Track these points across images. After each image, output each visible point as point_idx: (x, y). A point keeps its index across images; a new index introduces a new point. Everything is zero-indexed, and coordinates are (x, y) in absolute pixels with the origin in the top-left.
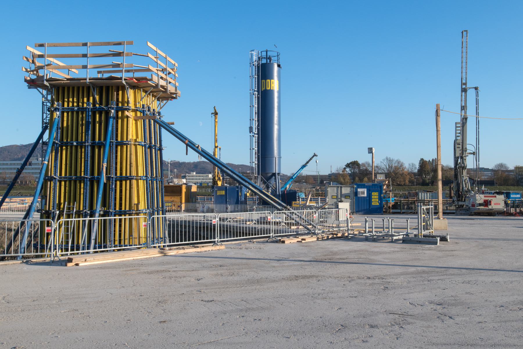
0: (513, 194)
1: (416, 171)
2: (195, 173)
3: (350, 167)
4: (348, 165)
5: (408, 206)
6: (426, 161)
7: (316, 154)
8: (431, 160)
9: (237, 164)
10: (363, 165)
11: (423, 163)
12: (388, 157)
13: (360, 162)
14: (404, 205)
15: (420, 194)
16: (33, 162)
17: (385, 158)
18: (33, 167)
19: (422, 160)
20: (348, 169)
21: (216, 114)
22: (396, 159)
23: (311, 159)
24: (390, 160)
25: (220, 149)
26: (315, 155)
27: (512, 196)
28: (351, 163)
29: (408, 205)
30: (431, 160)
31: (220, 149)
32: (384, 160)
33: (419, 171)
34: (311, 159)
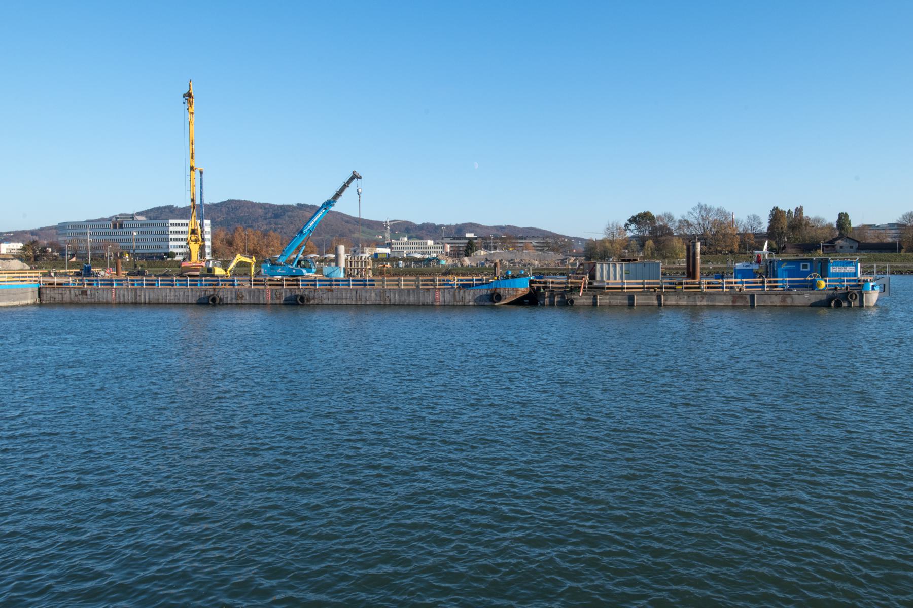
0: (835, 264)
1: (766, 230)
2: (406, 239)
3: (636, 222)
4: (633, 220)
5: (563, 297)
6: (782, 212)
7: (359, 172)
8: (793, 210)
9: (521, 226)
10: (660, 218)
11: (776, 215)
12: (703, 204)
13: (655, 213)
14: (552, 296)
15: (598, 266)
16: (125, 223)
17: (696, 205)
18: (125, 230)
19: (776, 209)
20: (632, 227)
21: (189, 95)
22: (716, 207)
23: (345, 186)
24: (704, 210)
25: (201, 173)
26: (355, 177)
27: (832, 269)
28: (639, 216)
29: (562, 295)
30: (793, 210)
31: (201, 173)
32: (693, 209)
33: (769, 229)
34: (345, 186)
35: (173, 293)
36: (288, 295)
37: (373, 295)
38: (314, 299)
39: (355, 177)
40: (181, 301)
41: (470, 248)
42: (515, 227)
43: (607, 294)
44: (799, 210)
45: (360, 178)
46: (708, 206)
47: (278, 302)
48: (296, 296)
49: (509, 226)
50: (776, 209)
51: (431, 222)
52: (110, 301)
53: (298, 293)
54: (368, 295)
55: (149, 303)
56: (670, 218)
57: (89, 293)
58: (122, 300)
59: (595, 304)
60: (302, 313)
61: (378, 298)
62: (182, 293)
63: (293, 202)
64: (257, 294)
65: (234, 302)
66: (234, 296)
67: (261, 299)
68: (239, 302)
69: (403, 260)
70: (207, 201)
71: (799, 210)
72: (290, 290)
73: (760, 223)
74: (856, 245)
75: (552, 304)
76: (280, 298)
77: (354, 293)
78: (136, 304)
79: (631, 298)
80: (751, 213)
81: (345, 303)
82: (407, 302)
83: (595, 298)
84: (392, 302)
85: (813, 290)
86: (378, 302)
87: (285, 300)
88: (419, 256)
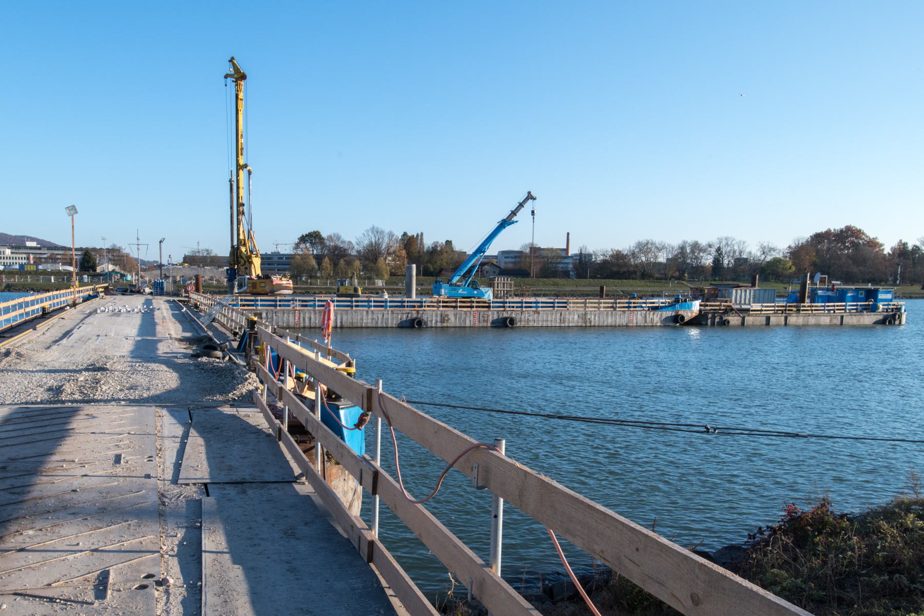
4: (303, 239)
14: (714, 318)
23: (521, 205)
26: (530, 197)
34: (521, 205)
35: (370, 316)
36: (496, 317)
37: (576, 317)
39: (530, 197)
40: (380, 325)
42: (6, 235)
43: (752, 315)
47: (485, 324)
48: (506, 318)
52: (292, 324)
53: (505, 315)
54: (571, 317)
55: (342, 327)
57: (264, 315)
58: (307, 324)
59: (743, 324)
60: (508, 335)
61: (580, 321)
62: (380, 316)
64: (463, 316)
65: (439, 325)
66: (439, 319)
67: (468, 321)
68: (445, 325)
69: (319, 278)
71: (449, 243)
72: (498, 312)
74: (497, 271)
75: (713, 324)
76: (487, 321)
77: (559, 315)
79: (768, 319)
81: (531, 324)
82: (605, 324)
83: (743, 318)
84: (593, 324)
85: (874, 311)
86: (580, 324)
87: (493, 322)
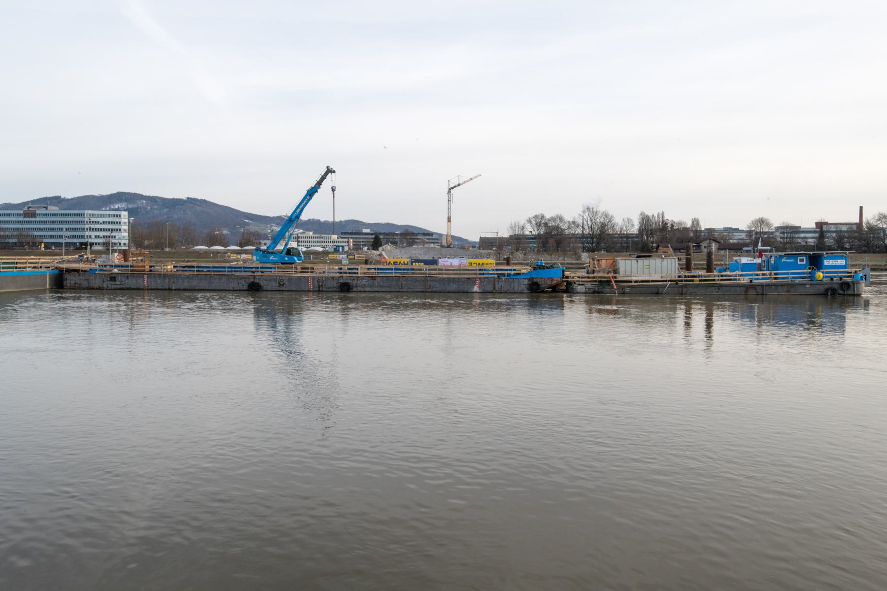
19: (642, 213)
26: (329, 171)
33: (639, 230)
38: (356, 286)
39: (329, 171)
41: (376, 243)
44: (696, 222)
45: (334, 172)
46: (595, 210)
49: (204, 202)
50: (642, 213)
51: (316, 217)
56: (561, 219)
63: (183, 196)
70: (337, 220)
71: (696, 222)
73: (633, 225)
78: (170, 289)
80: (625, 217)
88: (320, 249)
